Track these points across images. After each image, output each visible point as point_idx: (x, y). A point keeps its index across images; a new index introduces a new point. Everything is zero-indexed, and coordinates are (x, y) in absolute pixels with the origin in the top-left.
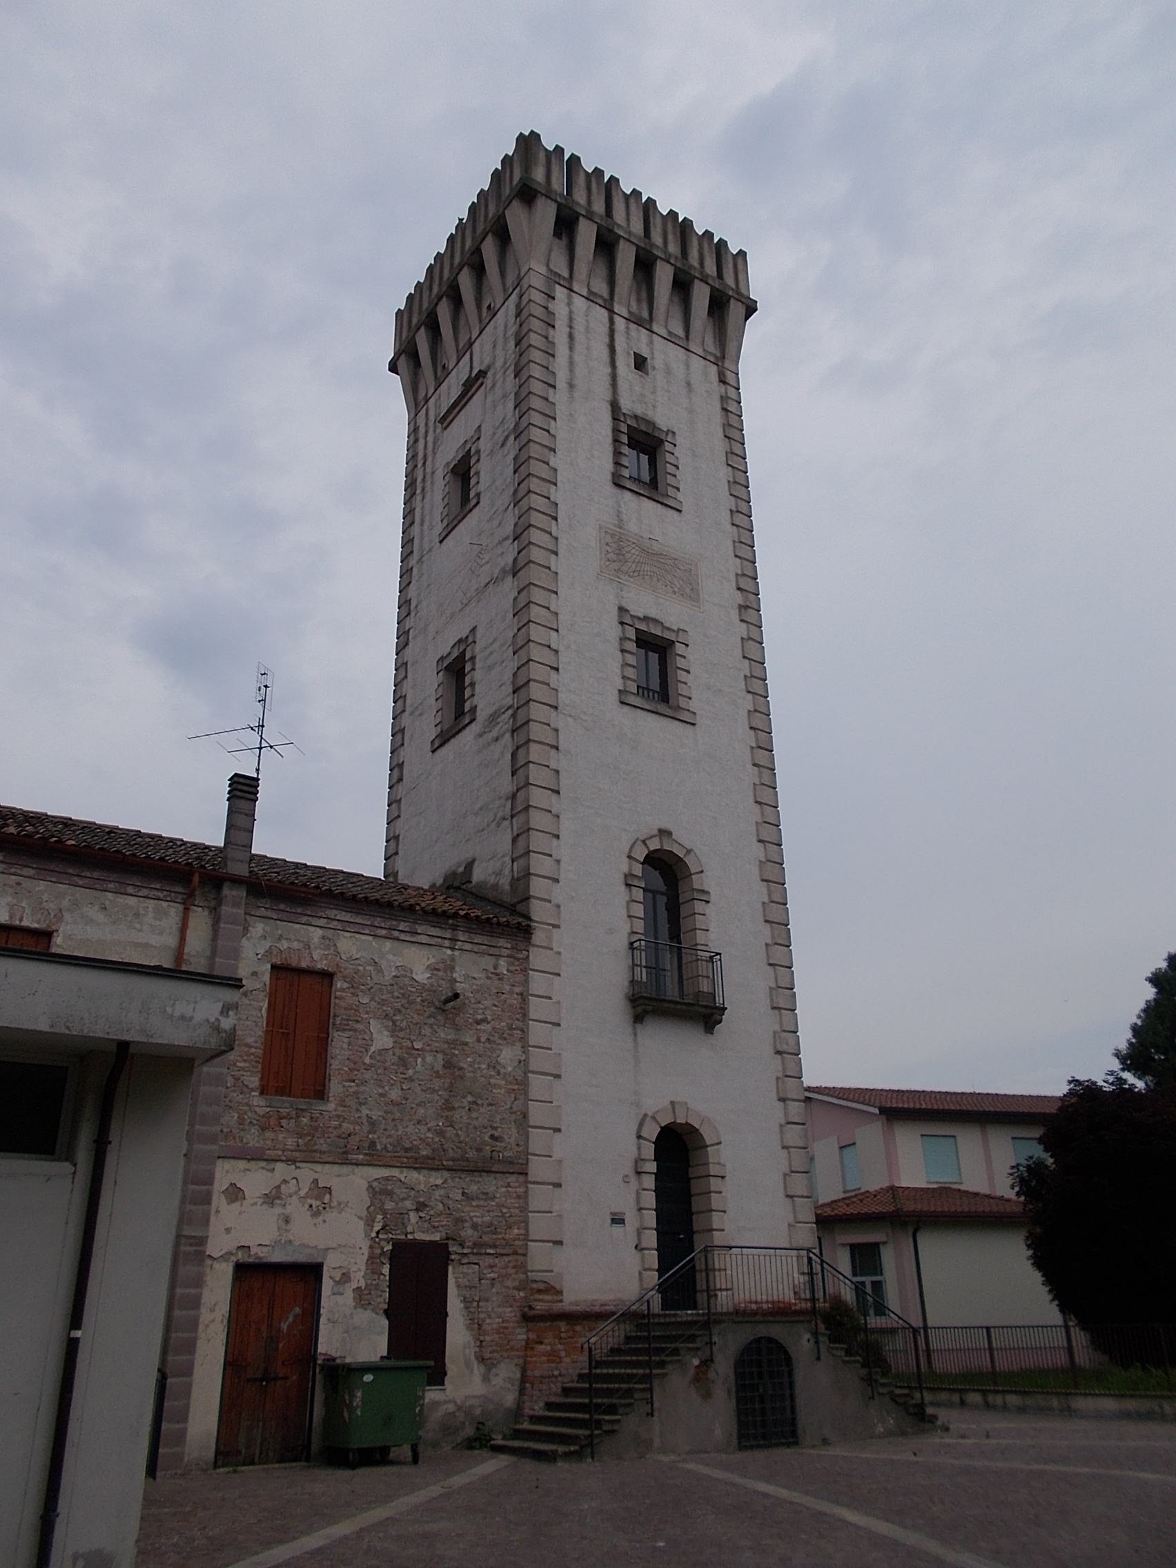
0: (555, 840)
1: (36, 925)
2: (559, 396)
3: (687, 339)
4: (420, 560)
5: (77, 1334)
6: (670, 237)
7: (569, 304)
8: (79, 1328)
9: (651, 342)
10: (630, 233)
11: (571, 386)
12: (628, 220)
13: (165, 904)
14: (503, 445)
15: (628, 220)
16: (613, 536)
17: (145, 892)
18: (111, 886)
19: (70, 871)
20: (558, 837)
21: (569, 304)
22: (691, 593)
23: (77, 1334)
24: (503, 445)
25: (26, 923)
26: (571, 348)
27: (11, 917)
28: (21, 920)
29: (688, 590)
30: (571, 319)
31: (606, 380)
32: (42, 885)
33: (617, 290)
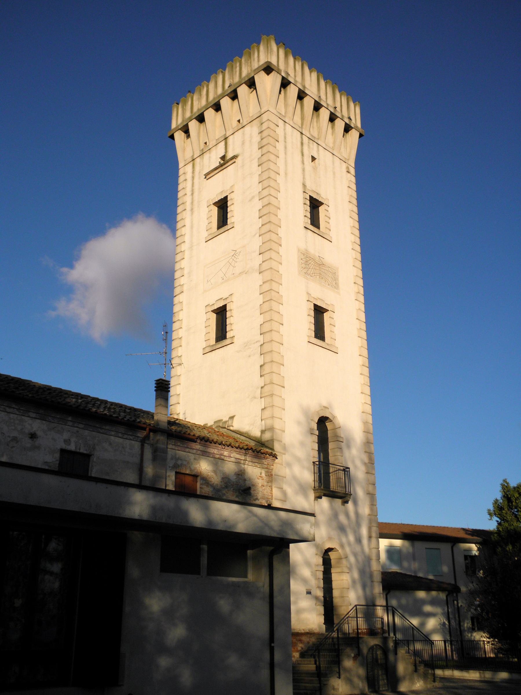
0: (283, 411)
1: (85, 452)
2: (280, 179)
3: (302, 128)
4: (191, 248)
5: (272, 645)
6: (329, 95)
7: (285, 130)
8: (273, 642)
9: (318, 150)
10: (328, 105)
11: (286, 174)
12: (326, 99)
13: (133, 442)
14: (250, 200)
15: (326, 99)
16: (304, 254)
17: (125, 436)
18: (113, 433)
19: (97, 426)
20: (284, 409)
21: (285, 130)
22: (335, 285)
23: (272, 645)
24: (250, 200)
25: (82, 451)
26: (286, 153)
27: (76, 448)
28: (80, 449)
29: (334, 284)
30: (285, 138)
31: (300, 171)
32: (86, 432)
33: (304, 123)
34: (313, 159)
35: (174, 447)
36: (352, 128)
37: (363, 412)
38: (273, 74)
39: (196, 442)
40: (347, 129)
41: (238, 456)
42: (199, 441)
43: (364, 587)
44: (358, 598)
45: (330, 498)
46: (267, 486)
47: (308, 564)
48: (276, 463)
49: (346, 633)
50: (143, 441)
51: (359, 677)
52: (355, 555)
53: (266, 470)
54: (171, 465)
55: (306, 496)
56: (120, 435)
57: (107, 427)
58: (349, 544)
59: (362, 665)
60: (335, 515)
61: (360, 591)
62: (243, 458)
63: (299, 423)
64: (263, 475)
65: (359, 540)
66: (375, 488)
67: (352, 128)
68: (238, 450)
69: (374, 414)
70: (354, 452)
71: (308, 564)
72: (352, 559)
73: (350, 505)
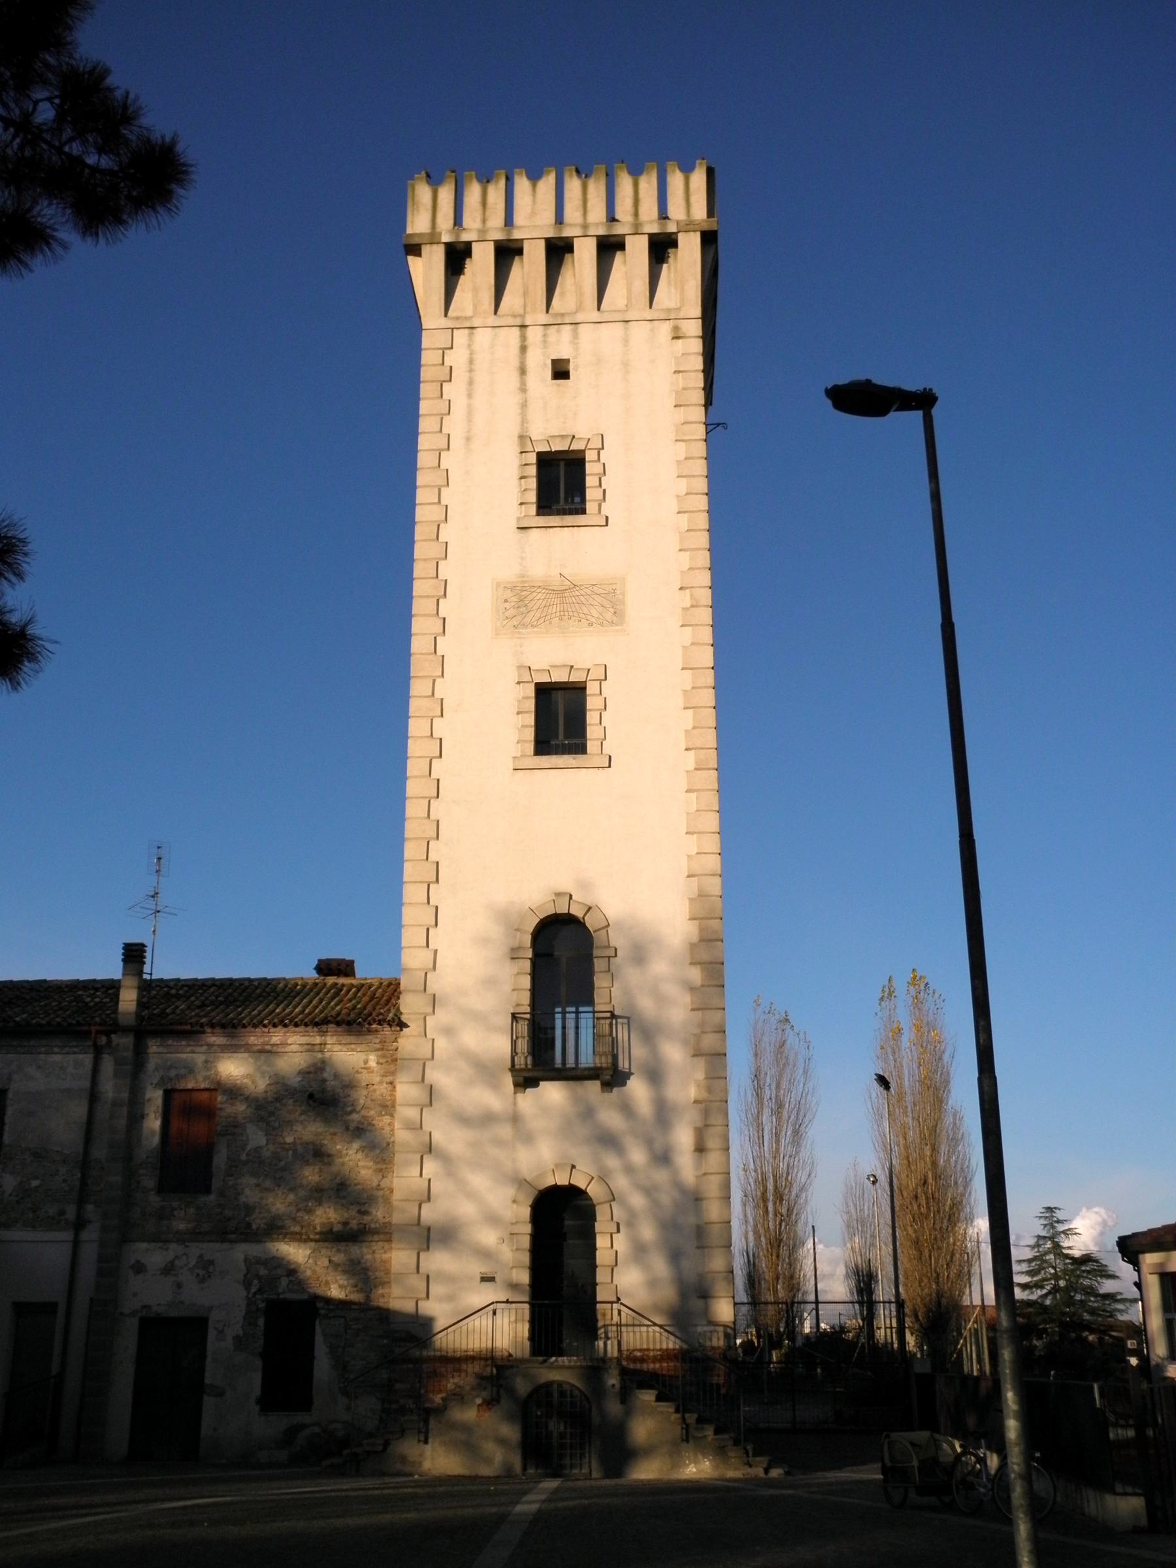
13: (81, 1056)
16: (513, 589)
17: (67, 1049)
34: (560, 372)
35: (161, 1049)
36: (676, 234)
37: (689, 876)
38: (425, 250)
39: (204, 1032)
40: (661, 248)
41: (304, 1040)
42: (209, 1030)
43: (675, 1257)
44: (652, 1283)
45: (571, 1083)
46: (381, 1082)
47: (493, 1220)
48: (408, 1037)
49: (402, 1351)
50: (98, 1052)
51: (502, 1442)
52: (649, 1191)
53: (380, 1053)
54: (155, 1082)
55: (495, 1086)
56: (56, 1050)
57: (32, 1043)
58: (629, 1169)
59: (510, 1418)
60: (588, 1113)
61: (661, 1266)
62: (318, 1040)
63: (484, 941)
64: (372, 1063)
65: (663, 1158)
66: (724, 1040)
67: (676, 234)
68: (302, 1028)
69: (727, 873)
70: (660, 967)
71: (493, 1220)
72: (637, 1201)
73: (637, 1089)
